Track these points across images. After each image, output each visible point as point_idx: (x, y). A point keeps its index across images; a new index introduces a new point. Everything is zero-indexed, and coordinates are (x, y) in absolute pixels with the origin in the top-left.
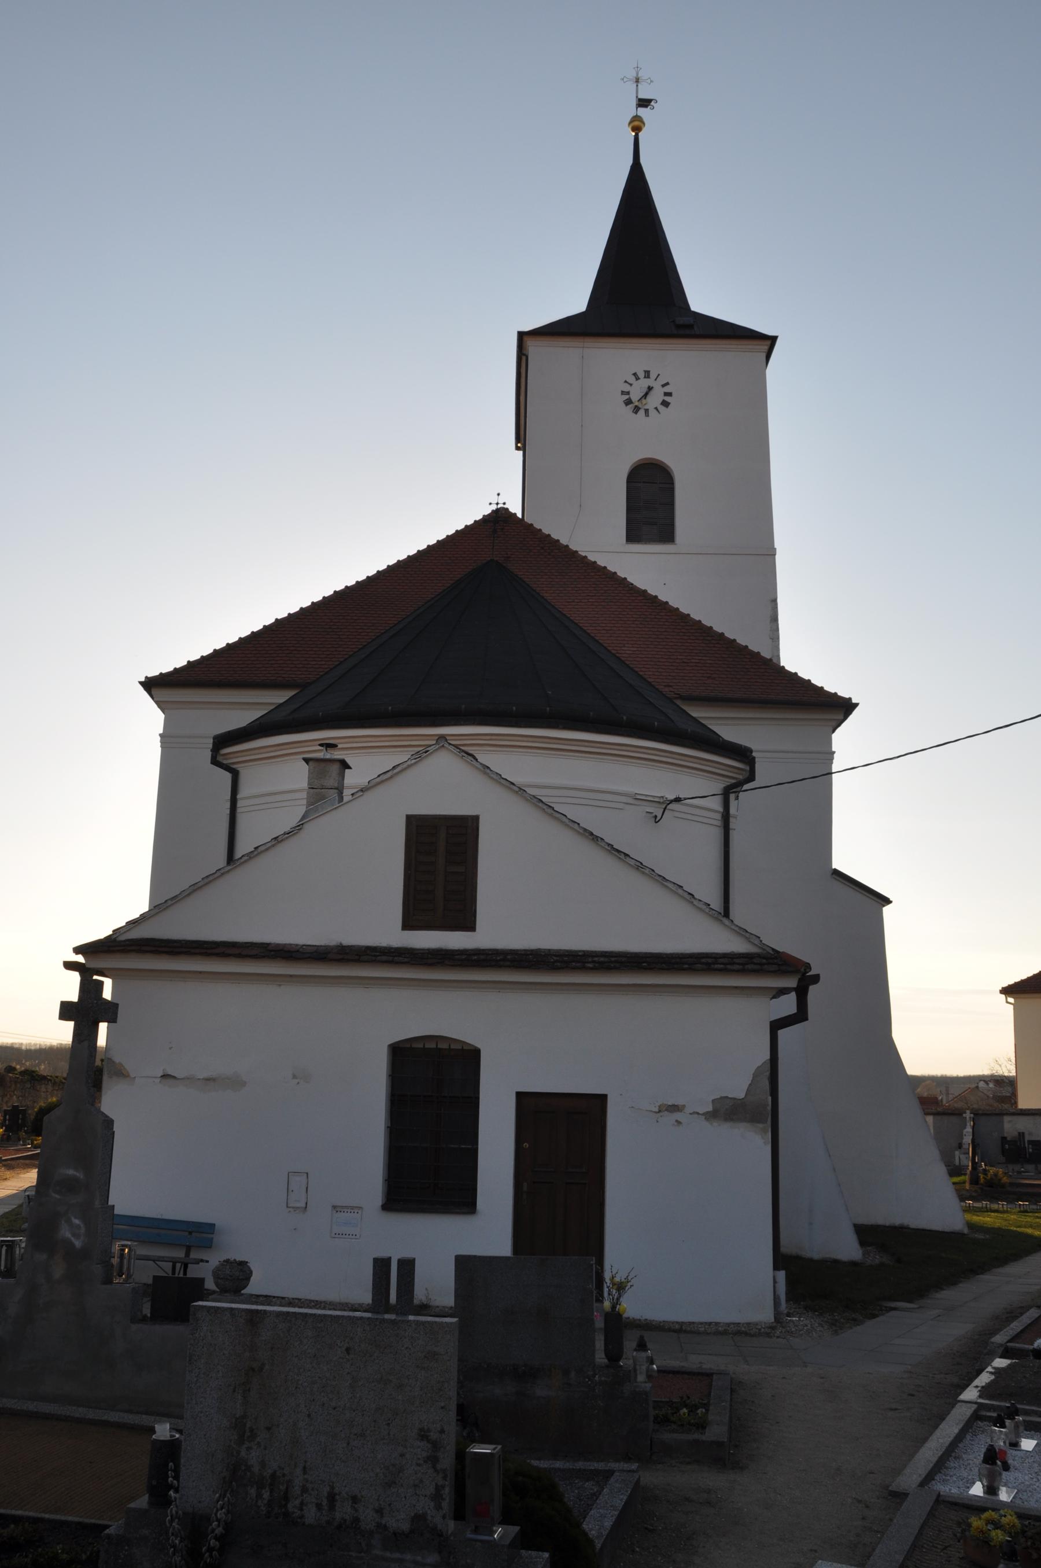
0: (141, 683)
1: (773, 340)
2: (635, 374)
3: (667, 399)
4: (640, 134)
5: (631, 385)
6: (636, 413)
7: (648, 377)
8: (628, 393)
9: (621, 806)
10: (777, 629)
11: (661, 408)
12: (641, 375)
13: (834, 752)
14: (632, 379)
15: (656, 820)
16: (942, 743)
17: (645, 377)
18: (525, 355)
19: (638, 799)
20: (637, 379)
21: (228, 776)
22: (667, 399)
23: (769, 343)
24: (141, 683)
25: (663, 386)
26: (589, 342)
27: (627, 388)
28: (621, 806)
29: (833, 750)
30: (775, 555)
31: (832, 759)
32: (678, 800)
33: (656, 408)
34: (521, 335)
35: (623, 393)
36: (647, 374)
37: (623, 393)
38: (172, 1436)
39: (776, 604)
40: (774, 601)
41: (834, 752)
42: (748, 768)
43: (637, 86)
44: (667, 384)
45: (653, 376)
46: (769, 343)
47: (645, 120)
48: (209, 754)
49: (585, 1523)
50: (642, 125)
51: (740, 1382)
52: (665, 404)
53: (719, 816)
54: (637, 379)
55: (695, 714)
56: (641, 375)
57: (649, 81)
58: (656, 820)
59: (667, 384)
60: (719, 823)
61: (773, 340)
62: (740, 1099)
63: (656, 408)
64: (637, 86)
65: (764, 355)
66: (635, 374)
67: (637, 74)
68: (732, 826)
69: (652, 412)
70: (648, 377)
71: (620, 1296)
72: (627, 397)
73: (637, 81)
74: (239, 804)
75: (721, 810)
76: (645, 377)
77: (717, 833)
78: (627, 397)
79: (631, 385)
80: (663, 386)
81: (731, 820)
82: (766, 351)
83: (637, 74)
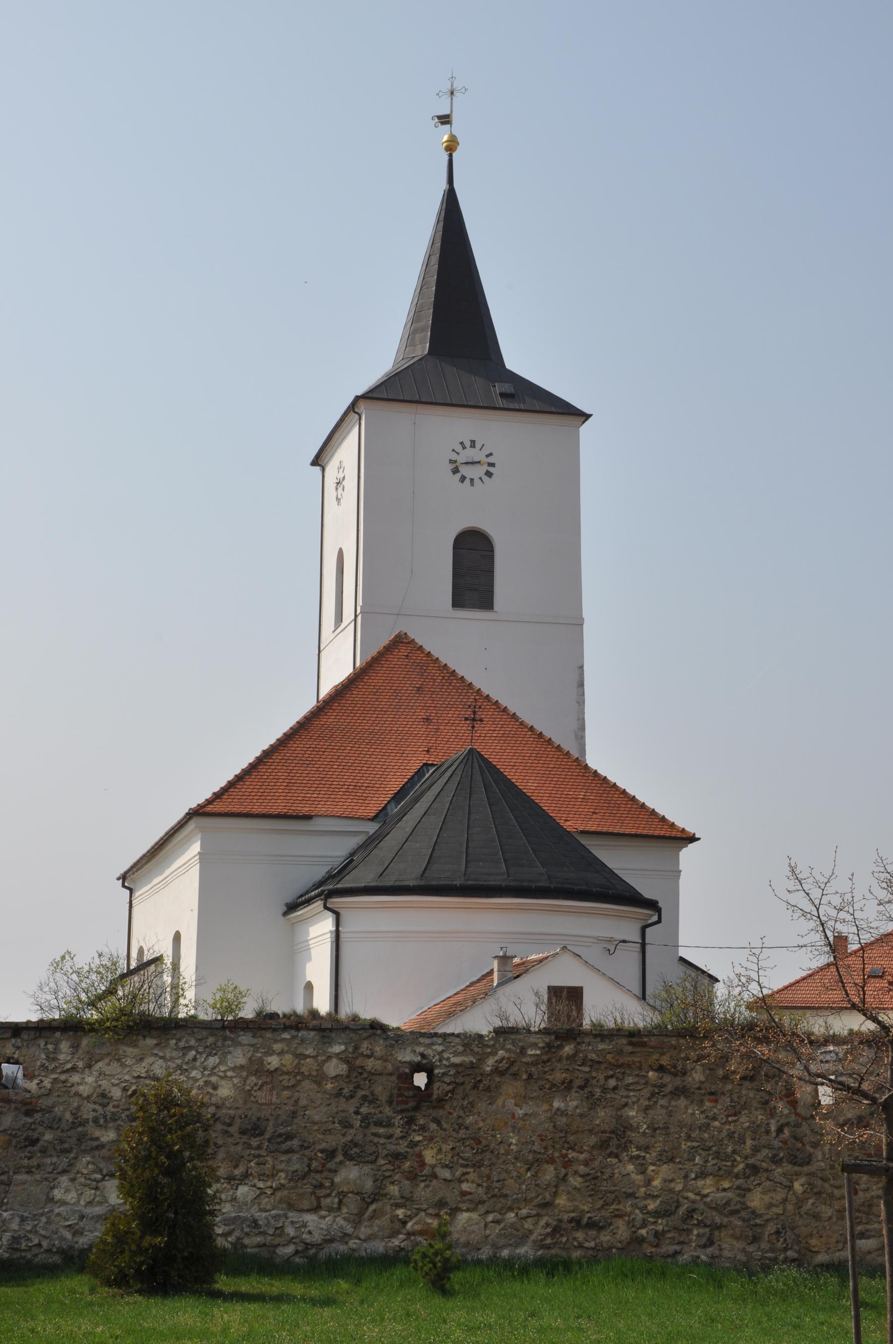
2: (462, 443)
3: (491, 469)
4: (454, 154)
5: (458, 454)
9: (590, 944)
10: (583, 694)
13: (681, 871)
17: (471, 447)
19: (599, 940)
20: (464, 448)
21: (128, 892)
23: (585, 418)
26: (422, 409)
28: (590, 944)
29: (680, 869)
30: (582, 625)
31: (679, 876)
32: (624, 941)
33: (480, 478)
37: (451, 461)
39: (583, 671)
40: (581, 667)
41: (681, 871)
43: (452, 99)
44: (491, 454)
47: (459, 140)
50: (455, 144)
52: (473, 444)
53: (639, 945)
54: (464, 448)
55: (583, 842)
59: (491, 454)
60: (639, 950)
63: (480, 478)
64: (452, 99)
66: (462, 443)
67: (452, 85)
71: (313, 1246)
73: (452, 93)
75: (640, 941)
76: (471, 447)
79: (458, 454)
83: (452, 85)
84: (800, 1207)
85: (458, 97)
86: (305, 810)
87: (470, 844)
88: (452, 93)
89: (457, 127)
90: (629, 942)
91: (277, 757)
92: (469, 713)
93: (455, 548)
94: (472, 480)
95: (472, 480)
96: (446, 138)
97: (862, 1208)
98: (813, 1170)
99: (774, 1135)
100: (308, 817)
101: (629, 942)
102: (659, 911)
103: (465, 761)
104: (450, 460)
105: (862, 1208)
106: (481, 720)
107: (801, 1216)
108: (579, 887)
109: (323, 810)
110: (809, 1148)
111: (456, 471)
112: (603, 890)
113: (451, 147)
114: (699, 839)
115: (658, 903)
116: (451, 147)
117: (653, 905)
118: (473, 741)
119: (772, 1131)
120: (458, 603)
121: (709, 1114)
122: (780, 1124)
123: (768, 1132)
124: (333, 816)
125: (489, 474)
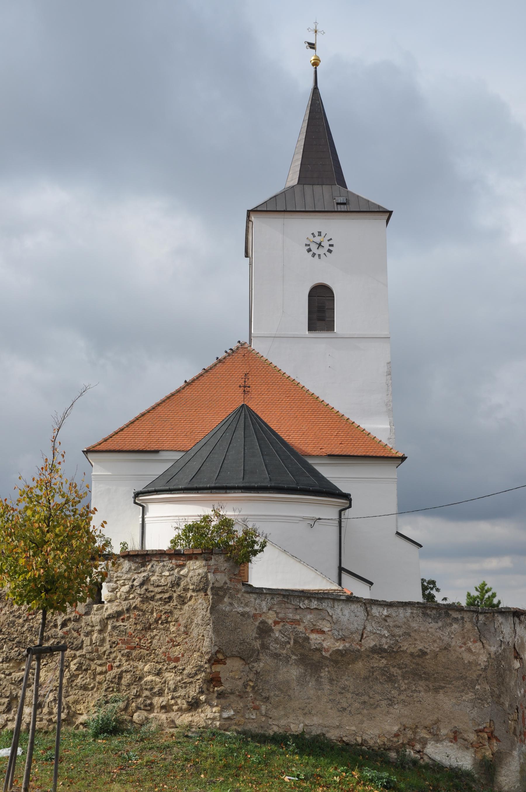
1: (391, 213)
2: (313, 234)
4: (318, 67)
6: (313, 257)
7: (320, 235)
8: (309, 245)
9: (297, 521)
11: (327, 254)
15: (312, 526)
16: (342, 558)
17: (318, 236)
18: (251, 221)
19: (304, 519)
21: (141, 508)
22: (331, 248)
23: (388, 214)
25: (329, 240)
28: (297, 521)
32: (320, 519)
33: (325, 254)
34: (248, 211)
35: (306, 245)
36: (320, 234)
37: (306, 245)
42: (348, 502)
43: (316, 35)
44: (331, 239)
45: (323, 234)
46: (388, 214)
47: (320, 59)
48: (133, 499)
53: (337, 522)
57: (322, 32)
58: (312, 526)
59: (331, 239)
61: (391, 213)
63: (325, 254)
64: (316, 35)
65: (385, 221)
67: (316, 27)
68: (342, 525)
69: (322, 256)
70: (320, 235)
72: (308, 247)
73: (316, 32)
74: (146, 520)
76: (318, 236)
77: (337, 529)
78: (308, 247)
80: (329, 240)
81: (342, 523)
82: (387, 219)
83: (316, 27)
84: (73, 681)
85: (319, 34)
86: (155, 448)
87: (225, 461)
88: (316, 32)
89: (320, 51)
90: (322, 519)
91: (148, 416)
92: (242, 382)
93: (309, 296)
94: (319, 255)
95: (319, 255)
96: (313, 58)
97: (113, 680)
98: (84, 653)
99: (59, 627)
100: (157, 452)
101: (322, 519)
102: (350, 500)
103: (237, 412)
104: (306, 244)
105: (113, 680)
106: (240, 386)
107: (72, 688)
108: (313, 488)
109: (166, 446)
110: (82, 637)
111: (309, 250)
112: (304, 487)
113: (315, 64)
114: (406, 458)
115: (350, 495)
116: (315, 64)
117: (347, 497)
118: (245, 400)
119: (59, 625)
120: (312, 328)
121: (15, 614)
122: (64, 619)
123: (55, 626)
124: (171, 450)
125: (330, 251)
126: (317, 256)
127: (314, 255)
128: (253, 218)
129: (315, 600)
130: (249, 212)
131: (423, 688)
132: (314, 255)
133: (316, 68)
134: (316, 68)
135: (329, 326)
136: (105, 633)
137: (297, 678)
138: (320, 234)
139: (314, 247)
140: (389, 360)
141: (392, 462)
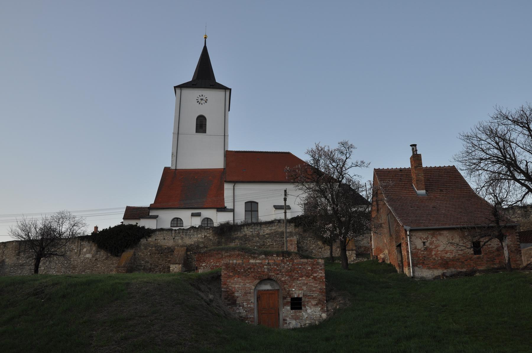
0: (375, 169)
2: (200, 96)
8: (198, 100)
12: (201, 96)
14: (199, 97)
24: (375, 169)
25: (206, 98)
27: (198, 99)
36: (202, 95)
37: (197, 100)
38: (521, 162)
44: (207, 98)
45: (203, 96)
49: (295, 238)
51: (187, 250)
54: (200, 96)
56: (201, 96)
59: (207, 98)
62: (447, 167)
66: (200, 96)
69: (203, 104)
74: (233, 201)
80: (206, 98)
120: (197, 131)
126: (201, 104)
127: (200, 103)
128: (176, 89)
129: (94, 246)
130: (175, 87)
131: (316, 173)
132: (200, 103)
133: (205, 39)
134: (205, 39)
135: (205, 132)
136: (300, 259)
137: (303, 247)
138: (202, 95)
139: (199, 100)
140: (227, 208)
141: (219, 90)
